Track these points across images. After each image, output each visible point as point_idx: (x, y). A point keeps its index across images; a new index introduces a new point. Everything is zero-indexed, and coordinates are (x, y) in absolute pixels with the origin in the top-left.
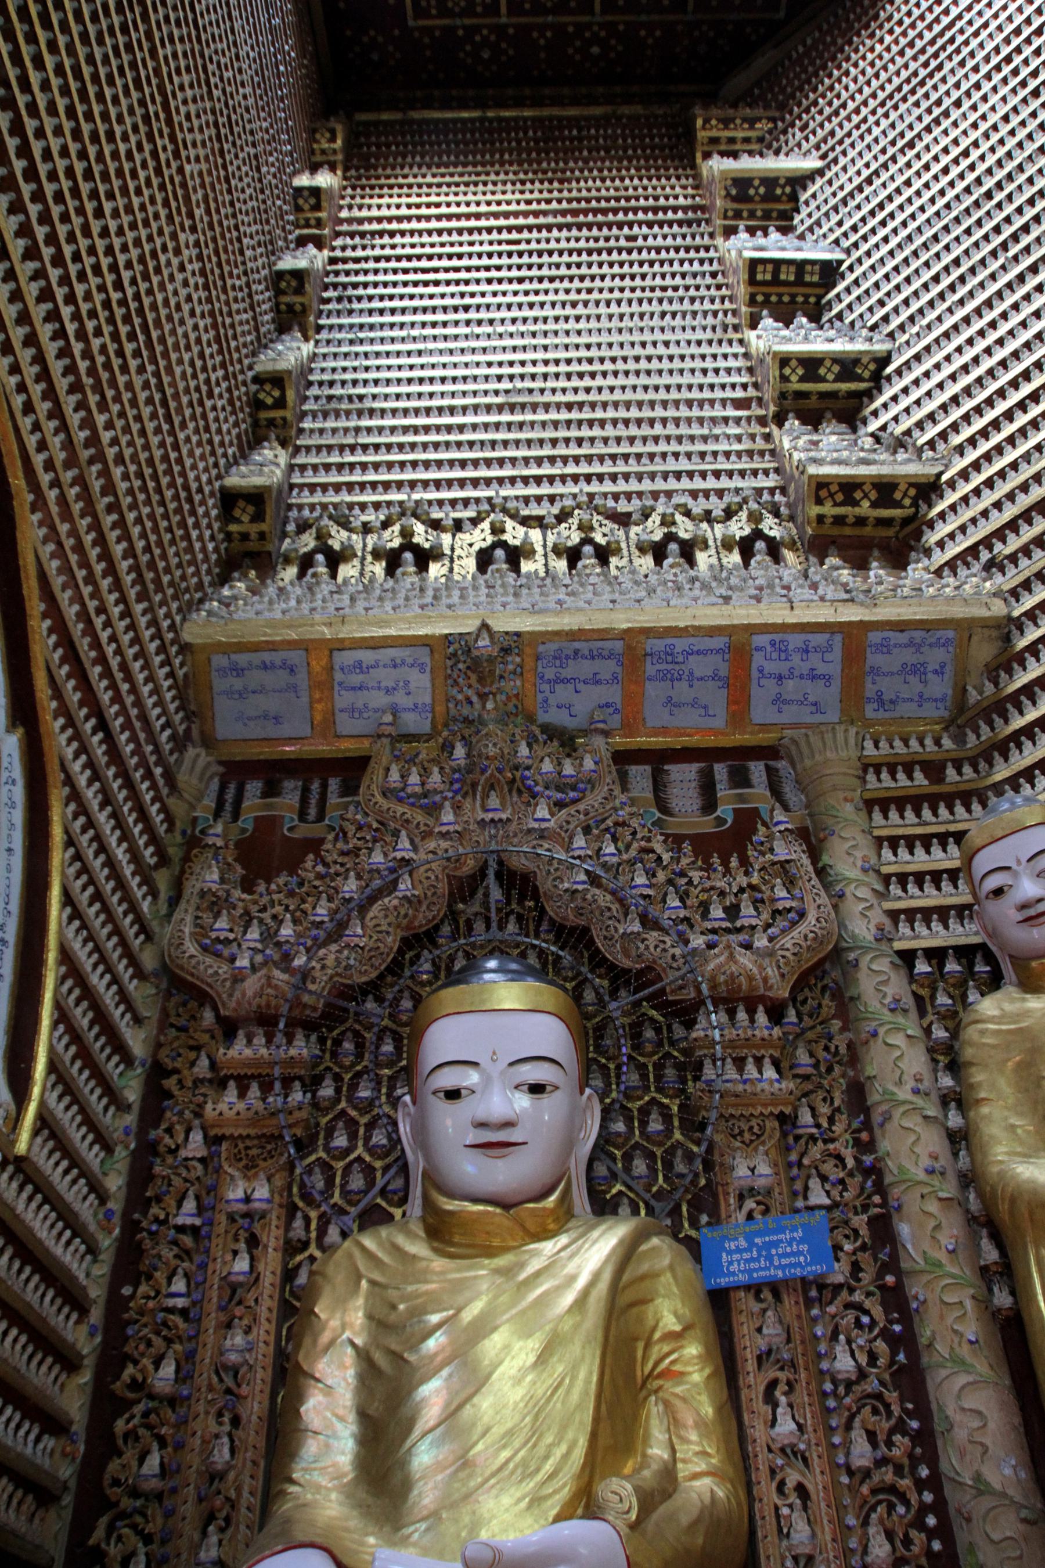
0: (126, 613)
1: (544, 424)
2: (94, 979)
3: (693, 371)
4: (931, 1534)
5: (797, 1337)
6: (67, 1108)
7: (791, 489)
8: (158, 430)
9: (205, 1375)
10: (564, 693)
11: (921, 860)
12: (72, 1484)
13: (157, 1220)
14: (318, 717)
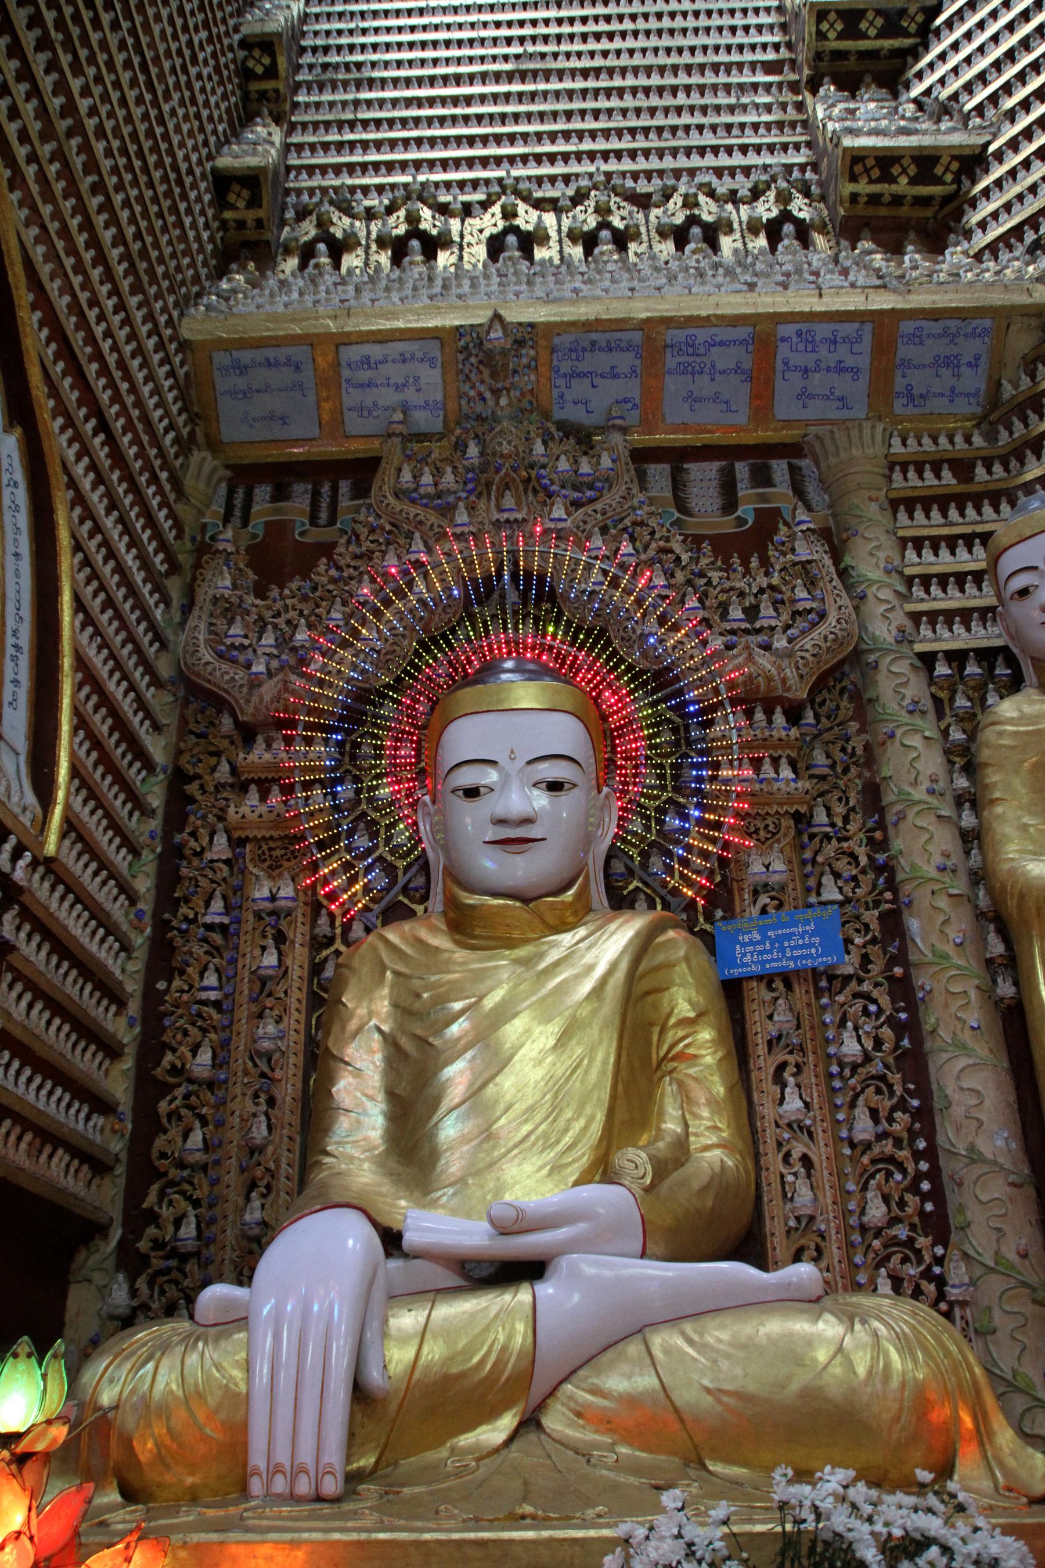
0: (121, 307)
1: (557, 94)
2: (111, 686)
3: (720, 29)
4: (924, 1197)
5: (806, 1023)
6: (92, 812)
7: (824, 165)
8: (140, 100)
9: (240, 1061)
10: (580, 388)
11: (945, 562)
12: (123, 1156)
13: (186, 919)
14: (326, 417)
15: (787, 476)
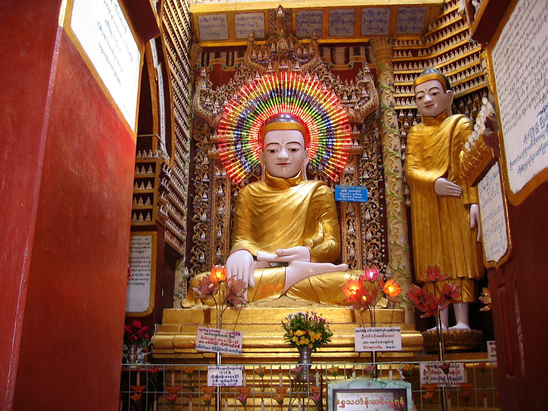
10: (304, 26)
13: (198, 180)
15: (364, 52)
